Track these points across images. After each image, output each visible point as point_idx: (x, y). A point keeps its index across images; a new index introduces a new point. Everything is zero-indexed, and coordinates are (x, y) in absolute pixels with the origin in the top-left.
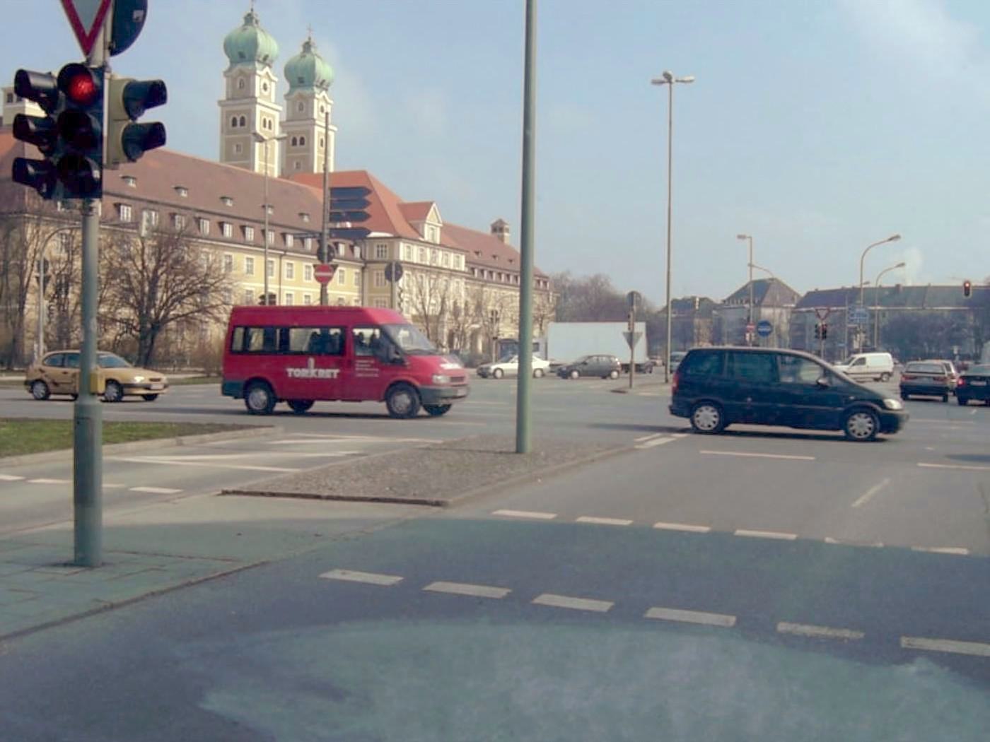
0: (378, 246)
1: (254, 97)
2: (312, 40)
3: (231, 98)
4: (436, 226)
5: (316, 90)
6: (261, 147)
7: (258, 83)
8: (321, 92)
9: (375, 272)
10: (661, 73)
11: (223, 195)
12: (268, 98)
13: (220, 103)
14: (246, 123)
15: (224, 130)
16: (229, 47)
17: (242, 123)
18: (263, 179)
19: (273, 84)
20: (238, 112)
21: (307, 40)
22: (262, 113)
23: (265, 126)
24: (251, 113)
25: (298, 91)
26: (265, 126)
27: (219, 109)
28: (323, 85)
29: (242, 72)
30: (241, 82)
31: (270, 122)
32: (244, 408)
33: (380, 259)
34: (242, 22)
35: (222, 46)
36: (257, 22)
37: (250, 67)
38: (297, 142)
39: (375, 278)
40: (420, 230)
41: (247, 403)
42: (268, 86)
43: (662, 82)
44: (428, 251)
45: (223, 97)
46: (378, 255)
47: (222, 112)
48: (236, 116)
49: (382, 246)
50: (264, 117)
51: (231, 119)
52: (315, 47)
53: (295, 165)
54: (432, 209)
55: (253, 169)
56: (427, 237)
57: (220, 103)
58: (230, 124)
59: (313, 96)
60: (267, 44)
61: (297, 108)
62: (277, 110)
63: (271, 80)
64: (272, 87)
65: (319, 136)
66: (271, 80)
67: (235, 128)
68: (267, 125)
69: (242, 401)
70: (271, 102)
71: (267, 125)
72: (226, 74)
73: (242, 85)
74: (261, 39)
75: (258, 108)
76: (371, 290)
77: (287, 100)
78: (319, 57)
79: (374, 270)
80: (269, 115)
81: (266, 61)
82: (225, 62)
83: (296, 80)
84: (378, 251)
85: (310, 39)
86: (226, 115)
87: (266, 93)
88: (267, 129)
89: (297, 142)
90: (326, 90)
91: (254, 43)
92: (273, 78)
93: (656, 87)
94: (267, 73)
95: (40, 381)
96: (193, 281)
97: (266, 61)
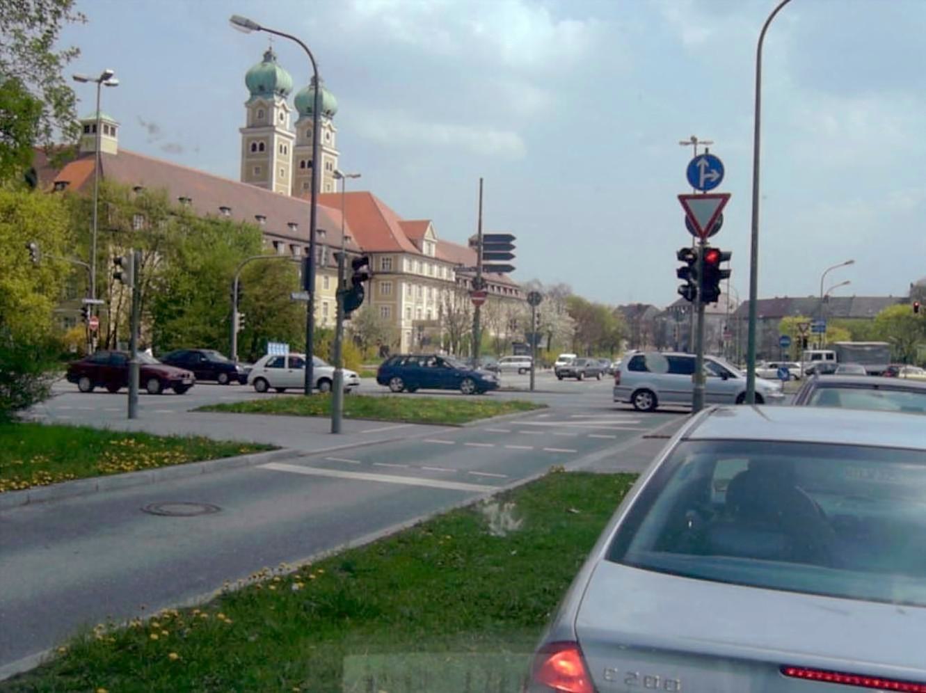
0: (383, 259)
1: (272, 126)
2: (273, 50)
3: (252, 126)
4: (433, 242)
5: (276, 98)
6: (333, 189)
7: (276, 113)
8: (281, 100)
9: (381, 282)
10: (689, 137)
11: (291, 222)
12: (283, 127)
13: (242, 130)
14: (265, 149)
15: (245, 155)
16: (250, 80)
17: (254, 147)
18: (277, 197)
19: (333, 134)
20: (257, 139)
21: (267, 49)
22: (325, 157)
23: (281, 151)
24: (270, 140)
25: (259, 98)
26: (281, 151)
27: (240, 136)
28: (329, 114)
29: (261, 104)
30: (261, 112)
31: (285, 148)
32: (77, 390)
33: (385, 270)
34: (262, 58)
35: (244, 80)
36: (275, 58)
37: (270, 100)
38: (308, 165)
39: (380, 286)
40: (419, 244)
41: (79, 387)
42: (284, 116)
43: (687, 144)
44: (426, 266)
45: (244, 125)
46: (384, 267)
47: (243, 140)
48: (256, 142)
49: (387, 259)
50: (281, 143)
51: (251, 145)
52: (322, 81)
53: (302, 185)
54: (429, 229)
55: (271, 189)
56: (425, 251)
57: (242, 130)
58: (250, 149)
59: (273, 104)
60: (284, 77)
61: (306, 135)
62: (336, 155)
63: (332, 131)
64: (288, 117)
65: (278, 142)
66: (332, 131)
67: (255, 153)
68: (283, 151)
69: (76, 385)
70: (286, 130)
71: (283, 151)
72: (248, 104)
73: (261, 114)
74: (279, 74)
75: (276, 136)
76: (376, 299)
77: (297, 128)
78: (326, 90)
79: (379, 280)
80: (285, 142)
81: (283, 93)
82: (247, 94)
83: (305, 110)
84: (383, 264)
85: (271, 48)
86: (246, 141)
87: (282, 122)
88: (283, 154)
89: (308, 165)
90: (331, 119)
91: (273, 76)
92: (334, 129)
93: (684, 147)
94: (283, 105)
95: (641, 391)
96: (583, 342)
97: (283, 93)
